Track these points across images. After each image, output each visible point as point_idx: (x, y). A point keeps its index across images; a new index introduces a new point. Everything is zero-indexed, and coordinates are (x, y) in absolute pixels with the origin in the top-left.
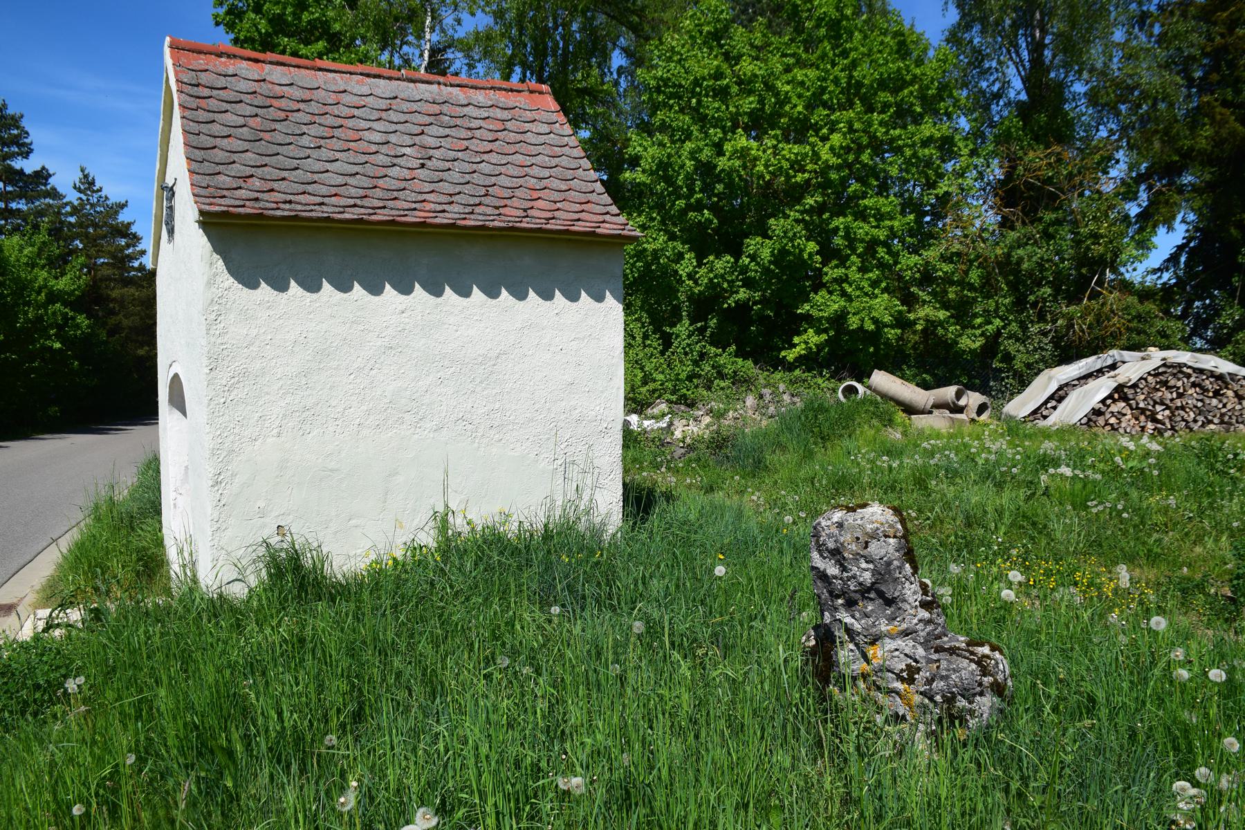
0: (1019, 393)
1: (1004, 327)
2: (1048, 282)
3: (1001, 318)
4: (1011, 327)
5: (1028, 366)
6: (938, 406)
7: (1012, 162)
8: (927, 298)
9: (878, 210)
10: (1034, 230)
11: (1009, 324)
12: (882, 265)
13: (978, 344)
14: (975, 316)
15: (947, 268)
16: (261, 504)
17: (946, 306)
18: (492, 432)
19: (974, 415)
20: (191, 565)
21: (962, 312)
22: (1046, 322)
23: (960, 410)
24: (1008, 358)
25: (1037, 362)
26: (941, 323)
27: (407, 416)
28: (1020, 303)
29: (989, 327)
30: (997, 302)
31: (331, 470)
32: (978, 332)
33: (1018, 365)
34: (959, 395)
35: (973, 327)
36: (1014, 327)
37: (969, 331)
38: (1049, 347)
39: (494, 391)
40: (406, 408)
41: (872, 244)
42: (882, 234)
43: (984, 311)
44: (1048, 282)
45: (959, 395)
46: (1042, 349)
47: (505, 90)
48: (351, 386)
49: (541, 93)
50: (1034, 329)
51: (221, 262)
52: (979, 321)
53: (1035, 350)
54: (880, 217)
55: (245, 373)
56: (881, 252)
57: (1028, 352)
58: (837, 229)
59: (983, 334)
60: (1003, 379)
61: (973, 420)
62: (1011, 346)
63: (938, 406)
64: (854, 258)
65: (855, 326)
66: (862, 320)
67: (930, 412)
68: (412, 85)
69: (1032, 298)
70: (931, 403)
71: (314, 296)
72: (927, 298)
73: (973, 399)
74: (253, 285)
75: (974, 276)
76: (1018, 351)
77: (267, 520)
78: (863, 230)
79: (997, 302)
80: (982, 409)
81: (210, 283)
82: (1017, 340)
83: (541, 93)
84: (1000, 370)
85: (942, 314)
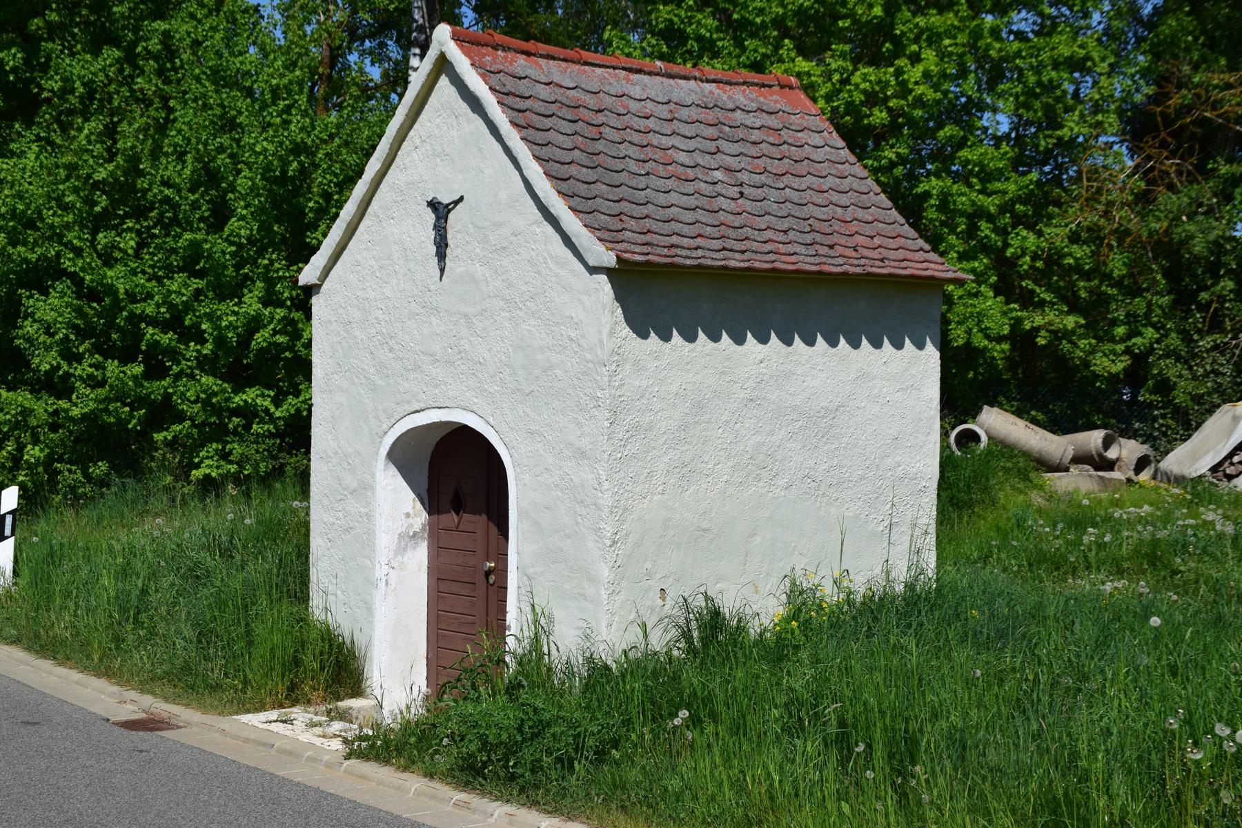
0: (1185, 439)
1: (1158, 341)
2: (1229, 272)
3: (1154, 326)
4: (1169, 341)
5: (1197, 399)
6: (1079, 459)
7: (1164, 82)
8: (1047, 297)
9: (983, 167)
10: (1206, 191)
11: (1166, 336)
12: (985, 248)
13: (1120, 366)
14: (1114, 323)
15: (1078, 251)
16: (648, 565)
17: (1074, 306)
18: (832, 490)
19: (1131, 474)
20: (540, 632)
21: (1095, 314)
22: (1223, 331)
23: (1110, 465)
24: (1164, 386)
25: (1209, 394)
26: (1067, 334)
27: (764, 473)
28: (1183, 300)
29: (1138, 340)
30: (1149, 304)
31: (704, 530)
32: (1120, 348)
33: (1180, 398)
34: (1107, 443)
35: (1112, 340)
36: (1174, 340)
37: (1107, 347)
38: (1227, 370)
39: (833, 447)
40: (763, 465)
41: (978, 213)
42: (991, 204)
43: (1128, 315)
44: (1229, 272)
45: (1107, 443)
46: (1217, 373)
47: (757, 85)
48: (720, 441)
49: (791, 88)
50: (1205, 343)
51: (619, 311)
52: (1120, 331)
53: (1206, 375)
54: (987, 176)
55: (638, 427)
56: (985, 228)
57: (1195, 378)
58: (927, 195)
59: (1128, 351)
60: (1155, 419)
61: (1129, 480)
62: (1172, 370)
63: (1080, 459)
64: (952, 239)
65: (961, 342)
66: (969, 332)
67: (1067, 470)
68: (671, 81)
69: (1204, 296)
70: (1070, 454)
71: (692, 346)
72: (1047, 297)
73: (1128, 450)
74: (644, 335)
75: (1117, 264)
76: (1180, 376)
77: (652, 583)
78: (965, 197)
79: (1149, 304)
80: (1142, 464)
81: (612, 333)
82: (1178, 359)
83: (791, 88)
84: (1151, 405)
85: (1070, 321)
